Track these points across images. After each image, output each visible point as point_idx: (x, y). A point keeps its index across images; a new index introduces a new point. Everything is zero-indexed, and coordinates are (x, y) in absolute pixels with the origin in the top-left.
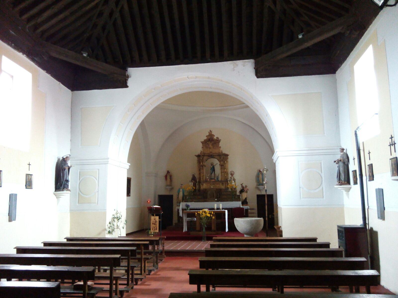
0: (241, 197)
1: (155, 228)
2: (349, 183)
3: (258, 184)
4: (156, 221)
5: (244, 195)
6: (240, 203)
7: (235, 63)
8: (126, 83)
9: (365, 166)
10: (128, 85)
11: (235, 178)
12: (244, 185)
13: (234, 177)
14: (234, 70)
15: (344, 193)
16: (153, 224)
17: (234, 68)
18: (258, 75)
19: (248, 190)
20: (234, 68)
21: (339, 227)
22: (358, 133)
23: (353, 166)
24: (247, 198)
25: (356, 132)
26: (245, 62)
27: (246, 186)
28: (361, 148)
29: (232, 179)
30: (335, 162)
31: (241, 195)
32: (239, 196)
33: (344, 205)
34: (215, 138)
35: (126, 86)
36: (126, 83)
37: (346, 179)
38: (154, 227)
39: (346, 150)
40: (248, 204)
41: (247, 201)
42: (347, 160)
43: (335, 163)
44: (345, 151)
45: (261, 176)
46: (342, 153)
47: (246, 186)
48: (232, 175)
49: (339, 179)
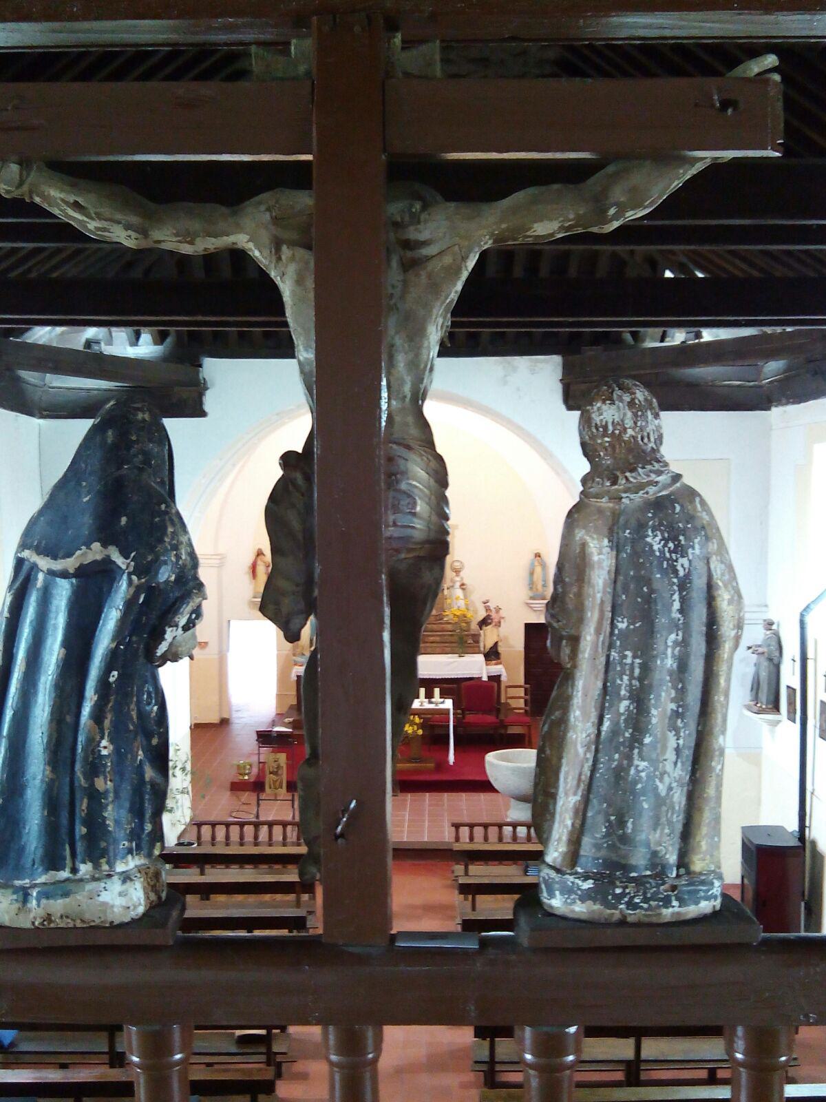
0: (482, 639)
1: (278, 783)
2: (776, 708)
3: (531, 595)
4: (279, 767)
5: (489, 637)
6: (481, 658)
7: (509, 363)
8: (201, 403)
9: (815, 703)
10: (207, 407)
11: (465, 582)
12: (492, 605)
13: (462, 579)
14: (505, 383)
15: (766, 728)
16: (271, 773)
17: (505, 376)
18: (570, 403)
19: (502, 621)
20: (505, 376)
21: (745, 830)
22: (808, 619)
23: (789, 677)
24: (500, 644)
25: (802, 615)
26: (537, 361)
27: (498, 610)
28: (810, 654)
29: (458, 584)
30: (749, 648)
31: (482, 632)
32: (476, 638)
33: (761, 748)
34: (485, 679)
35: (202, 414)
36: (199, 402)
37: (772, 698)
38: (275, 782)
39: (778, 625)
40: (502, 656)
41: (500, 649)
42: (777, 654)
43: (751, 651)
44: (774, 627)
45: (538, 570)
46: (768, 632)
47: (498, 610)
48: (457, 572)
49: (756, 699)
